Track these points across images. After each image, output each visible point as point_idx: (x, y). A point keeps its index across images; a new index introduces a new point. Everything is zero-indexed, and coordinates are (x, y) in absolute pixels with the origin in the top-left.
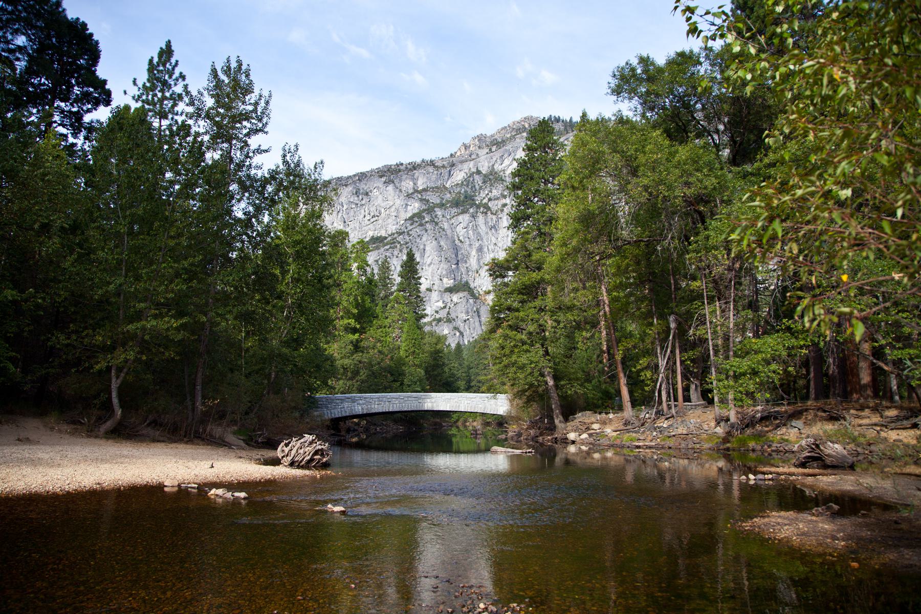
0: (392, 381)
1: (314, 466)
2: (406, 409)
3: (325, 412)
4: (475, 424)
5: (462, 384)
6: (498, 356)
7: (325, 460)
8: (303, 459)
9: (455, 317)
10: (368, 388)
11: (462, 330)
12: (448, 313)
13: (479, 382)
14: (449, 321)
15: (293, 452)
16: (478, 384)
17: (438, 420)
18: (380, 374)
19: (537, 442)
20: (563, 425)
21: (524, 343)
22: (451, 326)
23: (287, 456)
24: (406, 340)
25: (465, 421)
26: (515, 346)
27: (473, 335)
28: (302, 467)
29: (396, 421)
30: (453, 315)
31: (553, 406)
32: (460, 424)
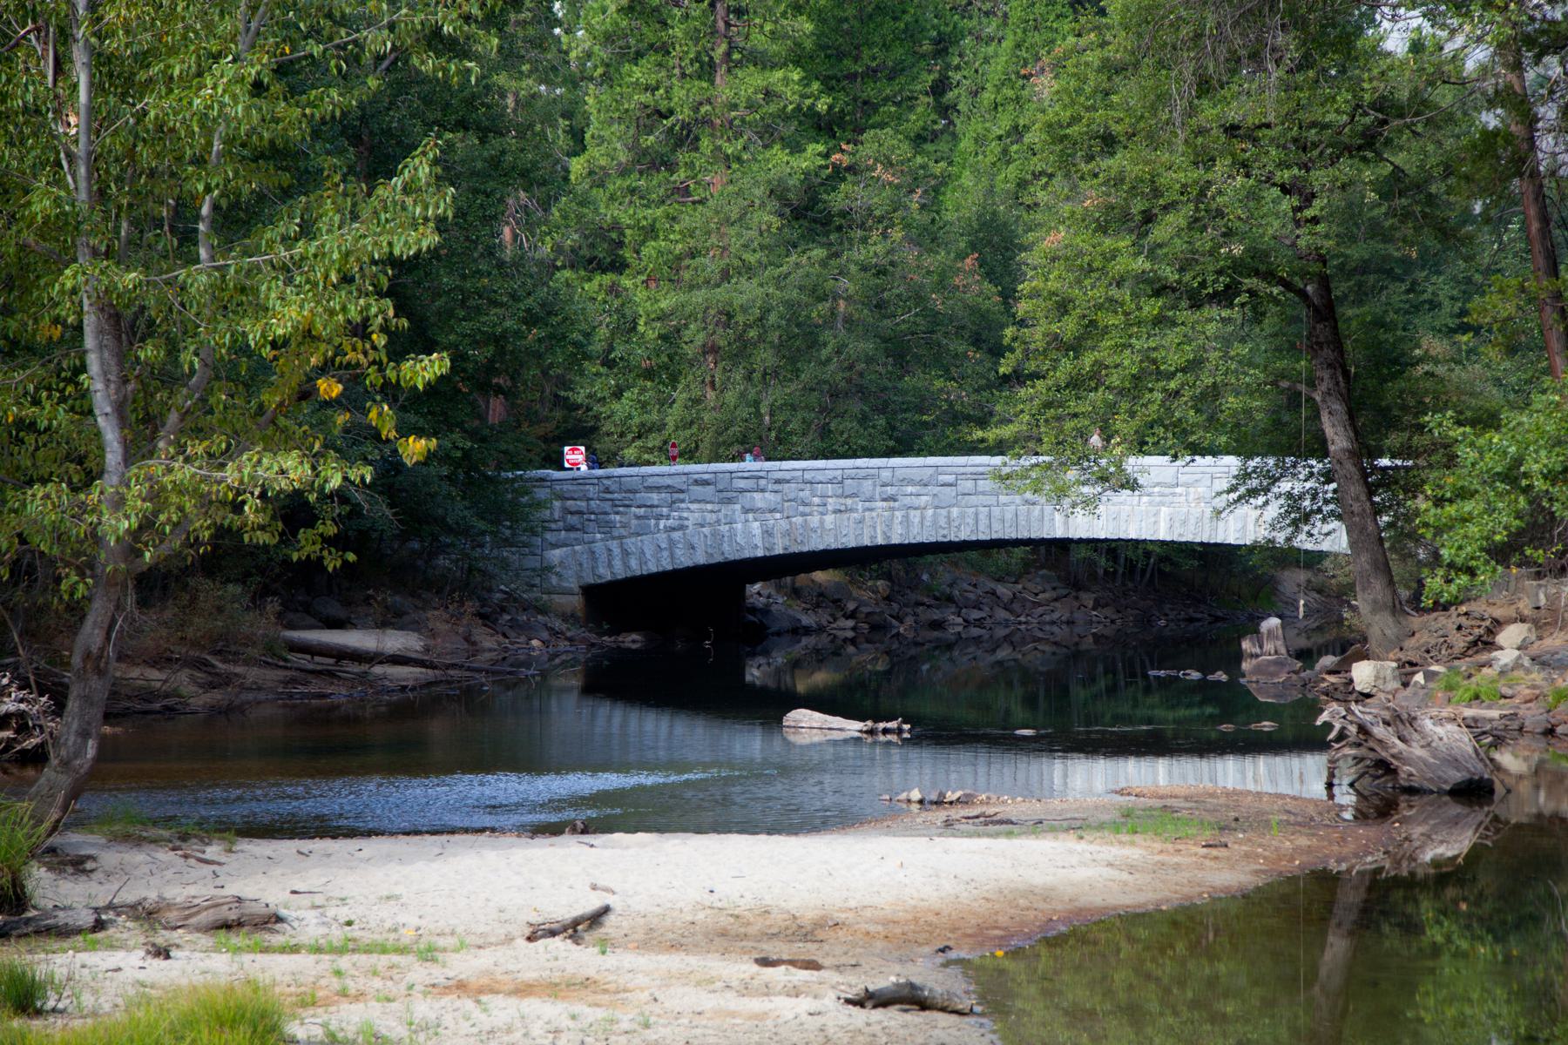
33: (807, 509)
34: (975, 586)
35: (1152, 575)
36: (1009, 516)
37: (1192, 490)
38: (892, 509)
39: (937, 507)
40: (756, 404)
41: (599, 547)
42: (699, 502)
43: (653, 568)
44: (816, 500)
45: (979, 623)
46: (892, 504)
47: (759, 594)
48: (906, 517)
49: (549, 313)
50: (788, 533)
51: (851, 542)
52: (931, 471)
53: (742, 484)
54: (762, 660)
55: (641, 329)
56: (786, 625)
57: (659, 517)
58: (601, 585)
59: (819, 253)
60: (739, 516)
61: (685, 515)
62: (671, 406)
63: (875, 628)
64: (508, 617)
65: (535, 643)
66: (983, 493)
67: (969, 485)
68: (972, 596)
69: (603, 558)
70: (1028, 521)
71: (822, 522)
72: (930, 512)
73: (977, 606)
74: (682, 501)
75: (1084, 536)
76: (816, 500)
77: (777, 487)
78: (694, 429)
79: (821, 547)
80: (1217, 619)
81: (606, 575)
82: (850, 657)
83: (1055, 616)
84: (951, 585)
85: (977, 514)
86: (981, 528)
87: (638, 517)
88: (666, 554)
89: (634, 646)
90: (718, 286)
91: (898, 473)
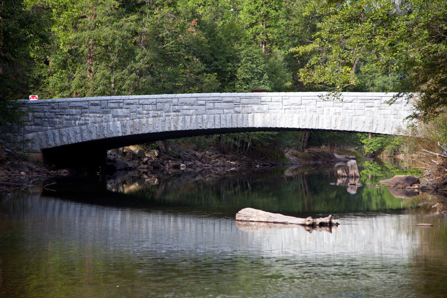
10: (153, 84)
25: (396, 152)
33: (141, 116)
34: (187, 152)
35: (249, 149)
36: (228, 118)
37: (307, 106)
38: (178, 116)
39: (197, 115)
40: (109, 78)
41: (49, 132)
42: (93, 113)
43: (73, 141)
44: (145, 112)
45: (190, 166)
46: (178, 113)
47: (110, 154)
48: (184, 119)
49: (30, 22)
50: (132, 126)
51: (160, 130)
52: (195, 99)
53: (112, 105)
54: (112, 181)
55: (61, 47)
56: (123, 167)
57: (76, 120)
58: (50, 148)
59: (134, 17)
60: (111, 119)
61: (87, 118)
62: (73, 79)
63: (155, 168)
64: (9, 162)
65: (23, 173)
66: (217, 109)
67: (211, 105)
68: (187, 156)
69: (51, 137)
70: (237, 120)
71: (147, 121)
72: (194, 117)
73: (190, 160)
74: (86, 113)
75: (261, 126)
76: (145, 112)
77: (127, 106)
78: (83, 88)
79: (147, 132)
80: (273, 165)
81: (52, 144)
82: (145, 179)
83: (218, 164)
84: (179, 152)
85: (214, 117)
86: (217, 123)
87: (67, 120)
88: (79, 135)
89: (65, 175)
90: (94, 30)
91: (180, 100)
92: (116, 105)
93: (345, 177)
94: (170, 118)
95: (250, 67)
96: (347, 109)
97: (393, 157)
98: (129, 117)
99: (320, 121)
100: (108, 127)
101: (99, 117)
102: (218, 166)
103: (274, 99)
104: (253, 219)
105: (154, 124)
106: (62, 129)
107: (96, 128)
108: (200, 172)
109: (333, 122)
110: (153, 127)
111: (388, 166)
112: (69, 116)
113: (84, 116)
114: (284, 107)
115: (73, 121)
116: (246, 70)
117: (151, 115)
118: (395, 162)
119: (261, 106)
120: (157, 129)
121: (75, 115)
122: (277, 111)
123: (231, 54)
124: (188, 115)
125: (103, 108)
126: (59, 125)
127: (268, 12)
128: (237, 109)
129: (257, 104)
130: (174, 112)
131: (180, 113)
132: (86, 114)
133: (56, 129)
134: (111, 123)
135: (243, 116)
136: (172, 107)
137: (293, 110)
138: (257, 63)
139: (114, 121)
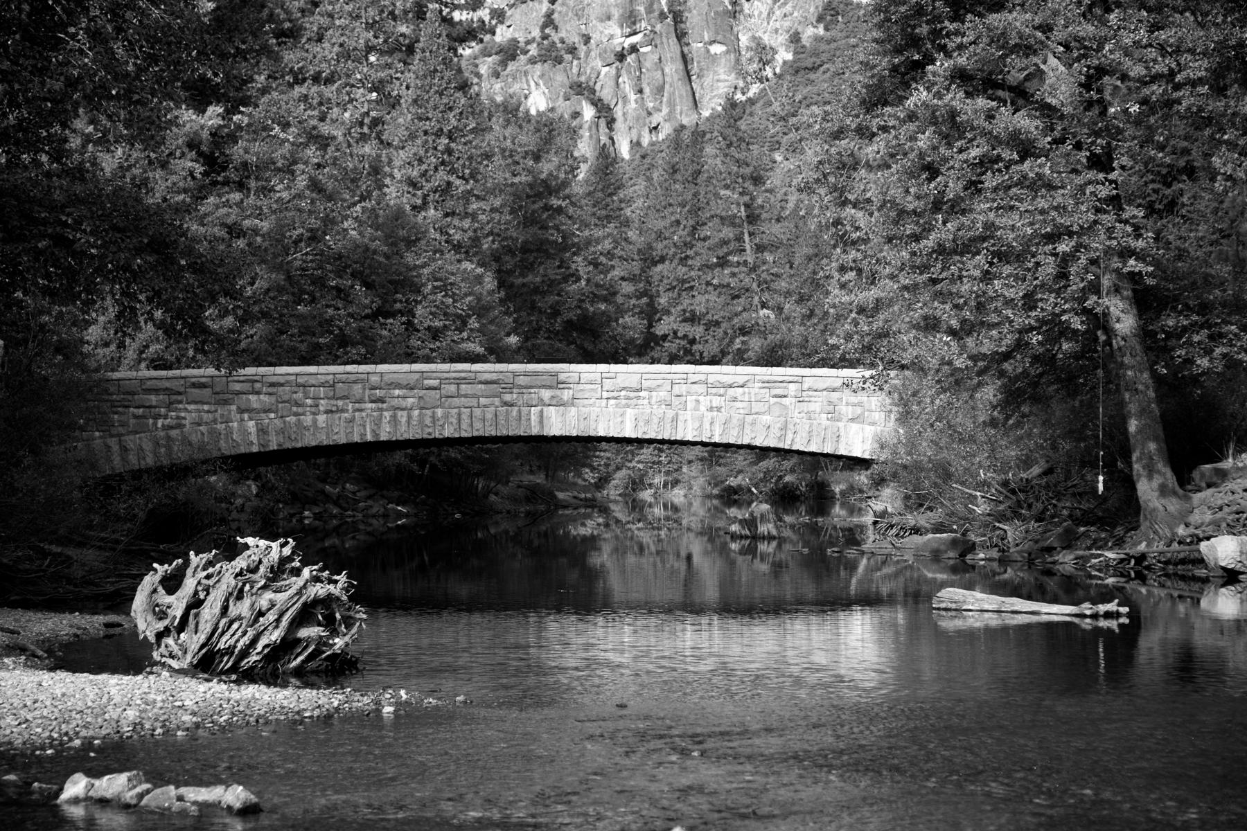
0: (374, 316)
1: (299, 673)
2: (448, 432)
3: (97, 443)
4: (677, 496)
5: (631, 324)
6: (911, 204)
7: (339, 642)
8: (254, 642)
9: (576, 39)
11: (606, 94)
12: (549, 21)
13: (692, 319)
14: (552, 55)
15: (209, 612)
16: (684, 329)
17: (539, 479)
18: (320, 282)
19: (1049, 573)
20: (1173, 505)
21: (1027, 150)
22: (560, 78)
23: (181, 627)
24: (412, 137)
25: (637, 483)
26: (985, 163)
27: (656, 119)
28: (249, 676)
29: (380, 484)
30: (568, 32)
31: (1133, 426)
32: (613, 491)
33: (300, 410)
36: (489, 416)
37: (654, 394)
38: (381, 410)
39: (422, 408)
42: (196, 403)
46: (380, 405)
48: (394, 417)
50: (281, 431)
53: (237, 387)
60: (235, 415)
61: (183, 414)
66: (466, 396)
67: (453, 388)
70: (507, 420)
71: (315, 422)
72: (416, 413)
74: (180, 402)
76: (309, 401)
77: (271, 390)
79: (314, 444)
83: (374, 510)
85: (459, 414)
86: (464, 426)
87: (136, 417)
91: (386, 377)
92: (247, 386)
93: (747, 537)
94: (364, 414)
95: (442, 302)
96: (735, 399)
97: (629, 495)
98: (275, 412)
99: (681, 425)
100: (229, 432)
101: (208, 412)
102: (374, 516)
103: (585, 377)
104: (970, 607)
105: (329, 427)
106: (126, 438)
107: (203, 434)
108: (336, 530)
109: (707, 425)
110: (328, 434)
111: (620, 516)
112: (141, 410)
113: (176, 410)
114: (605, 395)
115: (151, 421)
116: (434, 310)
117: (322, 408)
118: (634, 508)
119: (558, 392)
120: (335, 437)
121: (155, 407)
122: (591, 402)
123: (400, 274)
124: (403, 409)
125: (217, 393)
126: (120, 429)
127: (449, 184)
128: (507, 397)
129: (550, 387)
130: (372, 402)
131: (385, 406)
132: (181, 406)
133: (112, 436)
134: (235, 424)
135: (519, 411)
136: (367, 392)
137: (624, 402)
138: (454, 294)
139: (242, 420)
